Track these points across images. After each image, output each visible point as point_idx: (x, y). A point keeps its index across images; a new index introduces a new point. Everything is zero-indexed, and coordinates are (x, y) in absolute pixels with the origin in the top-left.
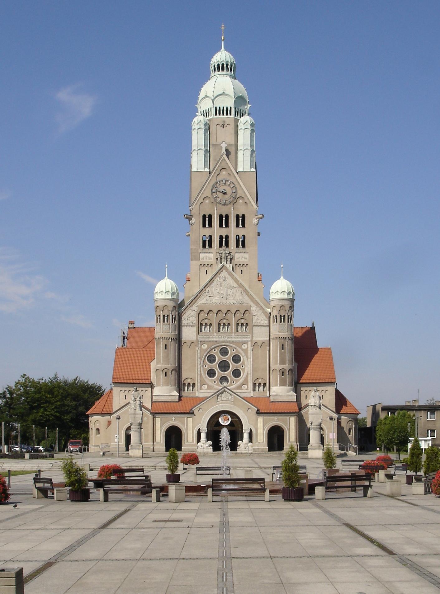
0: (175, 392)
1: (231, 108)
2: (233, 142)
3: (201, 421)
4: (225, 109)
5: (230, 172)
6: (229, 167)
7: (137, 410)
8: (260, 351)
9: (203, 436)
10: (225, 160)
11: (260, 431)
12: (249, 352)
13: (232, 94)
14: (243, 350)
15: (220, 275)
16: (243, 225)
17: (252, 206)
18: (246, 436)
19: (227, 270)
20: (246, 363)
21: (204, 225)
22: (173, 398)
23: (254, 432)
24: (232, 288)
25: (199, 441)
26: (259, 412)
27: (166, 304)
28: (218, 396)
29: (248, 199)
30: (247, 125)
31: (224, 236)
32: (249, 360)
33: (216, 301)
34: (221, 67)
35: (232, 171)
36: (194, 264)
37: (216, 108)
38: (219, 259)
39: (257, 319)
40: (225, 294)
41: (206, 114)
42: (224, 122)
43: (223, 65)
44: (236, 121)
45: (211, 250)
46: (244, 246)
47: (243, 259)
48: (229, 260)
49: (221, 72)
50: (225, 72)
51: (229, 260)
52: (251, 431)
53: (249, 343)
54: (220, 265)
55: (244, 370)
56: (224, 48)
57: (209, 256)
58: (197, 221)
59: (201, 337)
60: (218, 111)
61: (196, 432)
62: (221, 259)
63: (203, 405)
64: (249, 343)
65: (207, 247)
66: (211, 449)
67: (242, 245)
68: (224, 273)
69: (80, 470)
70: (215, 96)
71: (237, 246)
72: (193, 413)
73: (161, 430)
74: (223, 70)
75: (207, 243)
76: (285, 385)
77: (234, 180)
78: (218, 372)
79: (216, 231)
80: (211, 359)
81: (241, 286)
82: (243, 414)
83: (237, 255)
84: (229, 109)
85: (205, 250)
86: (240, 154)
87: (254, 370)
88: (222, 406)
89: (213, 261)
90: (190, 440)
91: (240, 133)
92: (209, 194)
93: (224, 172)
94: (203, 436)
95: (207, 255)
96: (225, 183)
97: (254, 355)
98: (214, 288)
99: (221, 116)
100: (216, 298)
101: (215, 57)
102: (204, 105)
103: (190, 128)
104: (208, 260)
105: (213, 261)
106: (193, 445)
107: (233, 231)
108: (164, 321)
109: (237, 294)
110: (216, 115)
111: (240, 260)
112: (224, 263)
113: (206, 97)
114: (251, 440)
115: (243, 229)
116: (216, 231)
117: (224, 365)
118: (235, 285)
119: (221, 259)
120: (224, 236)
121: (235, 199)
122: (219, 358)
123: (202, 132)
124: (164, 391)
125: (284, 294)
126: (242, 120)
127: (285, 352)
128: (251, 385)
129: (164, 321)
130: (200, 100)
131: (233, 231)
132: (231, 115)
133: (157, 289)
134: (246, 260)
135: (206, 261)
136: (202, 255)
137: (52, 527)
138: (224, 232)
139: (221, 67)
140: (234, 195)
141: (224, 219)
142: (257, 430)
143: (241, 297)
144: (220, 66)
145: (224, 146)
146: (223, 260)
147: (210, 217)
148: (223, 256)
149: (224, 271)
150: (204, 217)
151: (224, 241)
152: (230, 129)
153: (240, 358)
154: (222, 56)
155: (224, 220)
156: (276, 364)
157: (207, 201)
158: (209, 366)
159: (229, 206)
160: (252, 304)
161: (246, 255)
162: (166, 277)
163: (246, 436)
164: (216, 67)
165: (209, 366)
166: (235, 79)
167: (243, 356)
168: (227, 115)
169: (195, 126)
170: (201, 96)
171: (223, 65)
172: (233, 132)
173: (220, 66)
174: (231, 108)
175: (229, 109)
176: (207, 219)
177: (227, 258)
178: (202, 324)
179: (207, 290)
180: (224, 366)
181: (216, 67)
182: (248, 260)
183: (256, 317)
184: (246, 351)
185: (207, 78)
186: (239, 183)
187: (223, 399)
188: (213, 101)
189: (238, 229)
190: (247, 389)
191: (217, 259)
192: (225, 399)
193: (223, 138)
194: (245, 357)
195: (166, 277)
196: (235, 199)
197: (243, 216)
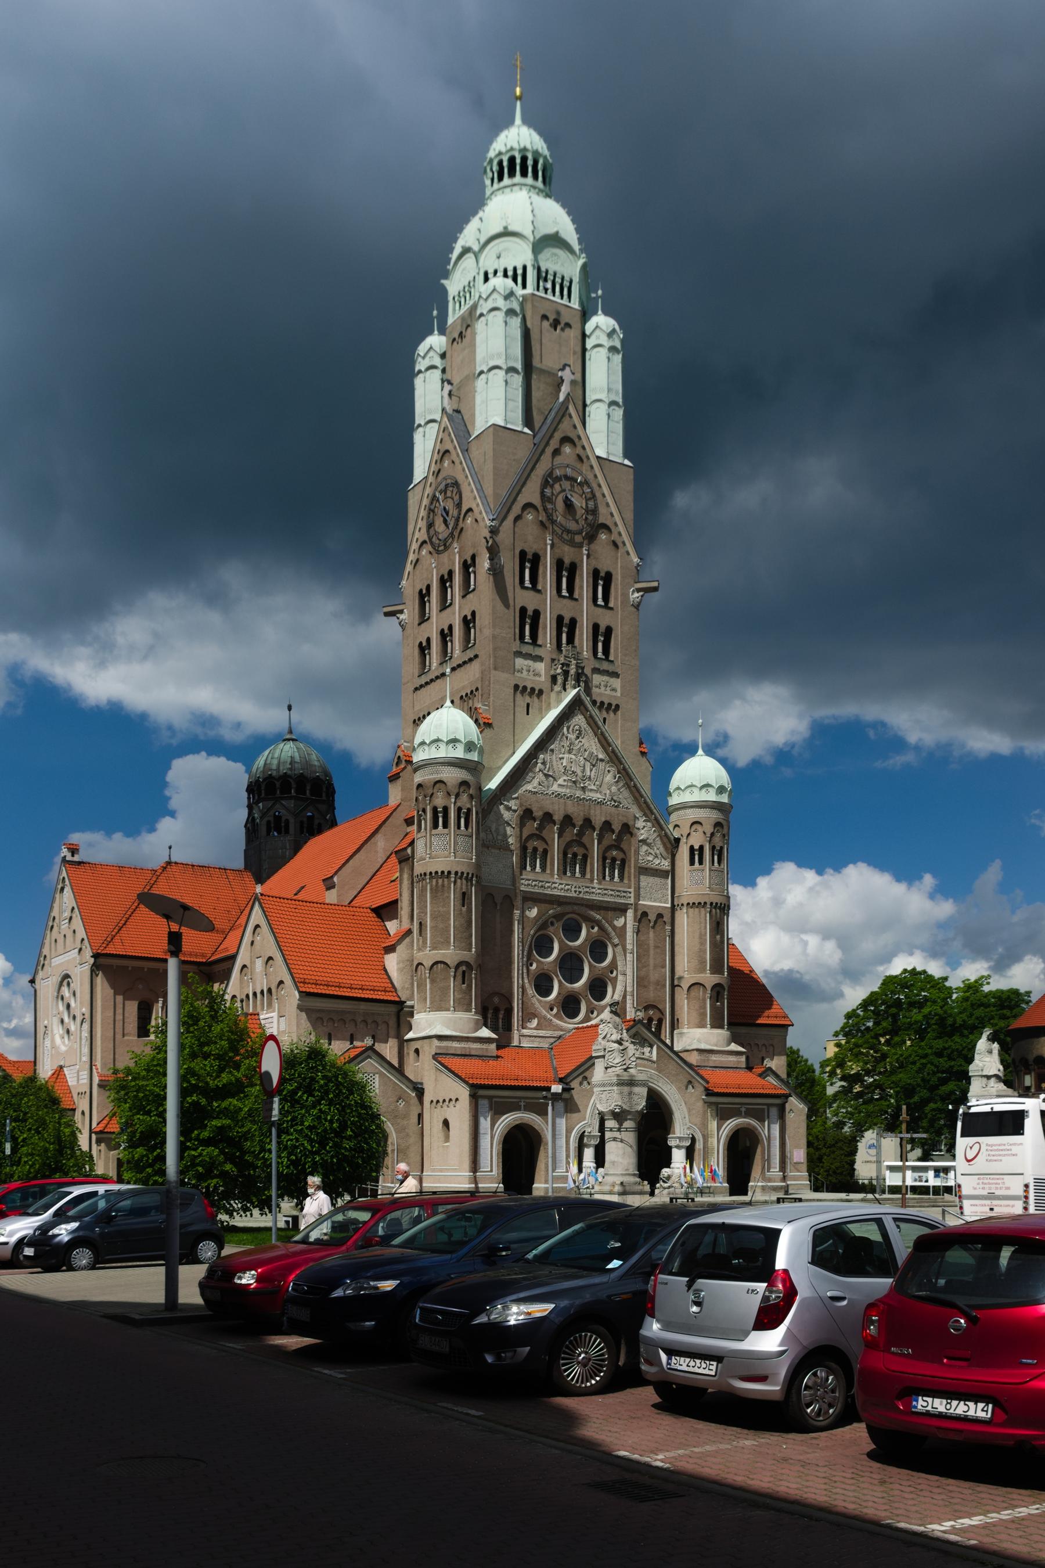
8: (651, 934)
23: (699, 1145)
24: (595, 762)
32: (629, 957)
33: (560, 790)
34: (516, 166)
38: (560, 679)
42: (558, 313)
43: (524, 159)
47: (608, 692)
50: (529, 180)
52: (693, 1140)
53: (630, 913)
55: (614, 981)
67: (604, 653)
70: (483, 240)
76: (721, 1027)
77: (590, 477)
82: (678, 1096)
87: (641, 982)
92: (536, 500)
97: (640, 944)
121: (595, 529)
125: (692, 793)
139: (516, 166)
142: (705, 1138)
150: (523, 554)
154: (519, 137)
156: (702, 970)
157: (530, 517)
164: (505, 164)
171: (512, 160)
181: (505, 164)
182: (619, 694)
184: (622, 932)
196: (595, 529)
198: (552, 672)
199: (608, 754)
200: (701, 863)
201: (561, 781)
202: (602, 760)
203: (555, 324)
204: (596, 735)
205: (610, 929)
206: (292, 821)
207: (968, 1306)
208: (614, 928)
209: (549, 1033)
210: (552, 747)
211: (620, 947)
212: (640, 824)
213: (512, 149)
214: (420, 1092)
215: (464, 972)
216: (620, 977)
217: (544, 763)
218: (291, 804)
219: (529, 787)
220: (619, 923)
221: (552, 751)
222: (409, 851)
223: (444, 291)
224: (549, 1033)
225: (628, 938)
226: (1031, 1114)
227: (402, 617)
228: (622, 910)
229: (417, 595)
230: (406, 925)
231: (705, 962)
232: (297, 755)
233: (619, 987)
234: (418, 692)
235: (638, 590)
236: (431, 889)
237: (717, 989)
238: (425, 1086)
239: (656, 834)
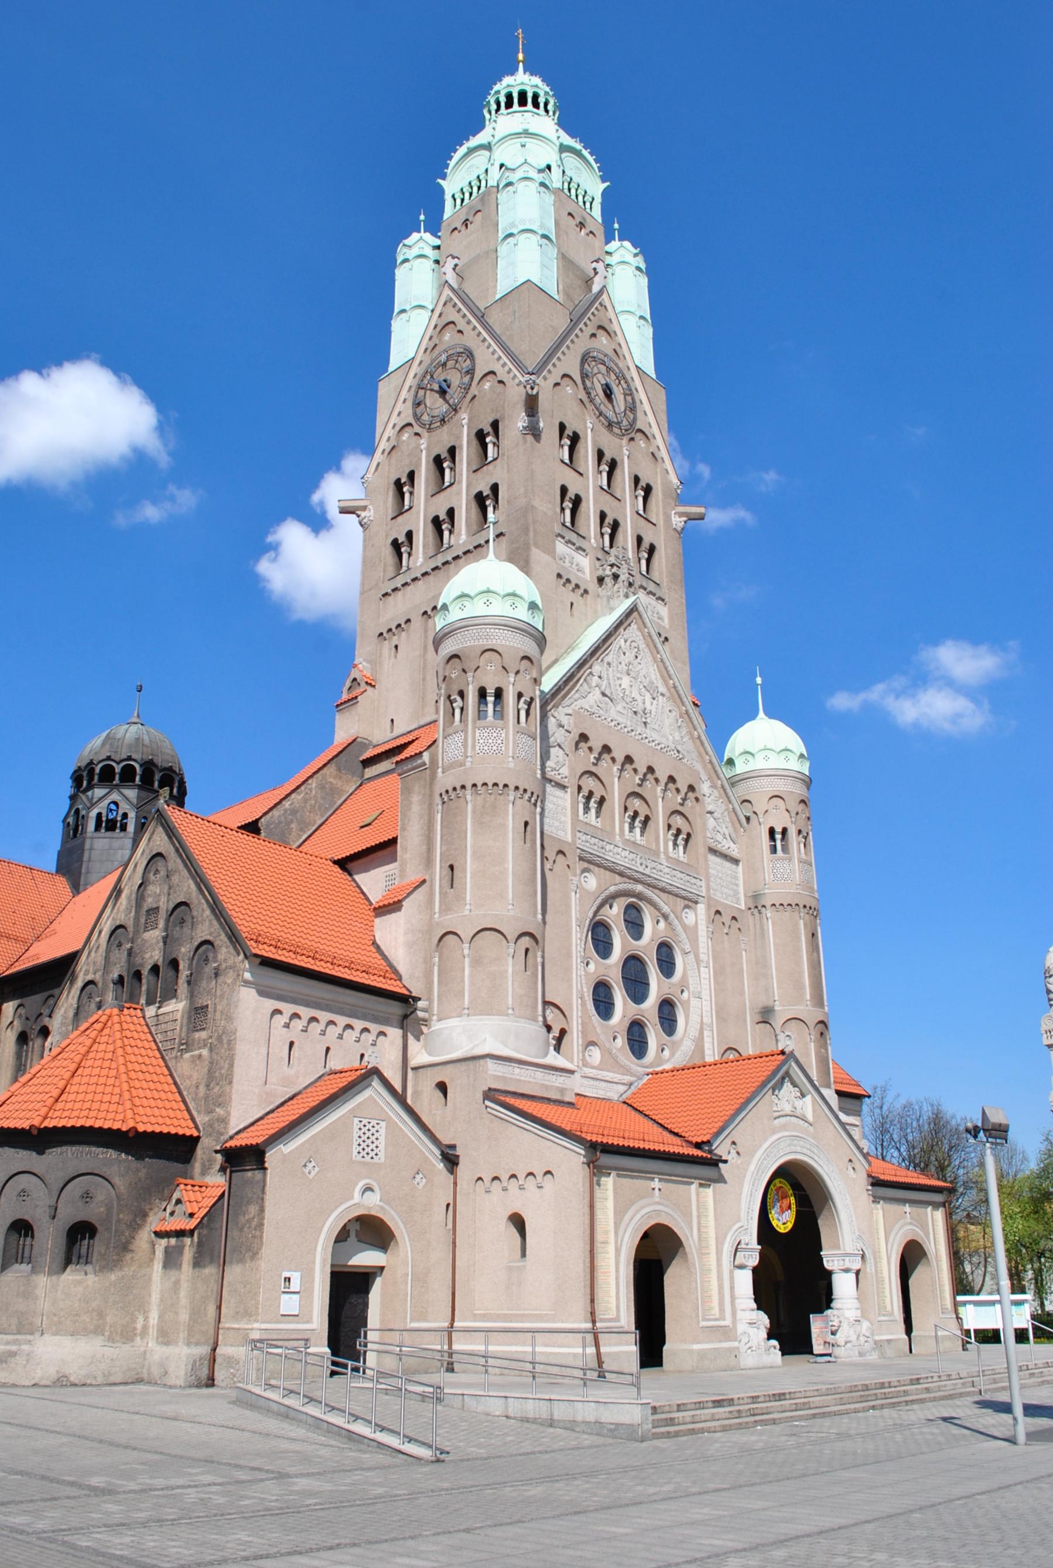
53: (701, 908)
184: (692, 932)
198: (600, 573)
199: (669, 689)
200: (785, 849)
201: (619, 708)
202: (663, 695)
204: (655, 660)
205: (679, 928)
206: (132, 815)
208: (685, 927)
209: (617, 1077)
211: (691, 956)
214: (451, 1160)
218: (132, 793)
220: (689, 917)
221: (609, 664)
222: (426, 756)
223: (441, 191)
224: (617, 1077)
225: (701, 945)
227: (363, 514)
228: (690, 902)
229: (392, 487)
230: (413, 876)
231: (803, 987)
232: (146, 737)
233: (695, 1018)
234: (389, 599)
235: (681, 515)
236: (474, 811)
238: (459, 1151)
239: (724, 807)
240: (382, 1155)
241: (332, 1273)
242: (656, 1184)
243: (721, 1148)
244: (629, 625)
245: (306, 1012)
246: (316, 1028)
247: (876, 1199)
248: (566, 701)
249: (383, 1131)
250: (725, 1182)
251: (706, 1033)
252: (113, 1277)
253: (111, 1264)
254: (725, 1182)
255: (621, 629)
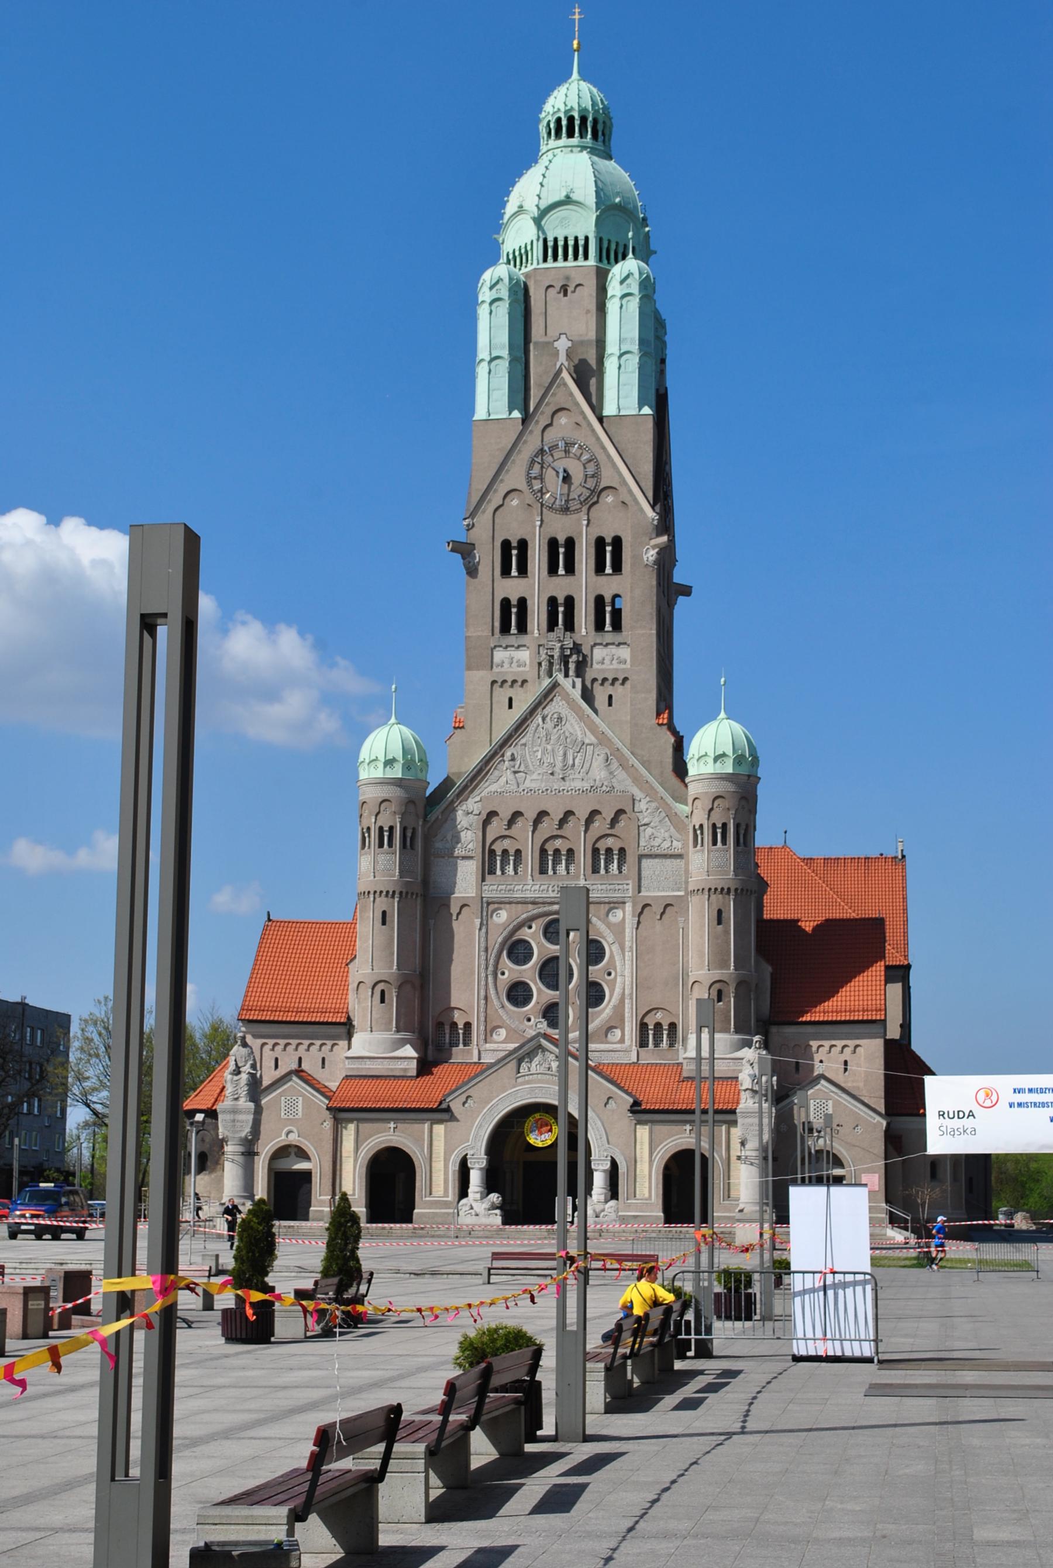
0: (408, 1047)
1: (587, 239)
2: (592, 335)
3: (471, 1136)
4: (571, 243)
5: (580, 419)
6: (577, 404)
7: (242, 1100)
9: (476, 1178)
10: (565, 384)
11: (643, 1168)
12: (627, 930)
13: (591, 200)
14: (609, 925)
15: (546, 712)
16: (617, 568)
17: (642, 510)
18: (599, 1180)
19: (567, 697)
20: (618, 964)
21: (506, 571)
22: (403, 1065)
23: (622, 1169)
25: (463, 1193)
26: (636, 1109)
27: (386, 796)
28: (520, 1061)
29: (630, 491)
30: (629, 286)
31: (561, 600)
33: (533, 785)
35: (585, 418)
36: (480, 678)
37: (545, 241)
39: (653, 837)
40: (559, 765)
41: (520, 257)
43: (571, 119)
44: (602, 276)
45: (524, 639)
46: (617, 626)
48: (572, 666)
49: (564, 140)
50: (575, 140)
51: (572, 666)
52: (614, 1164)
53: (629, 907)
54: (546, 682)
56: (579, 72)
57: (518, 658)
58: (488, 558)
59: (493, 889)
60: (552, 250)
61: (454, 1167)
62: (551, 664)
63: (477, 1091)
64: (629, 907)
65: (514, 630)
66: (496, 1218)
68: (557, 706)
69: (496, 1330)
71: (599, 626)
72: (448, 1110)
73: (356, 1160)
74: (570, 134)
75: (512, 617)
77: (591, 442)
78: (539, 990)
79: (583, 585)
80: (518, 951)
81: (603, 740)
83: (598, 653)
84: (581, 243)
85: (511, 640)
86: (611, 366)
87: (639, 984)
88: (532, 1089)
89: (528, 670)
90: (438, 1190)
91: (612, 307)
92: (522, 485)
93: (562, 420)
94: (476, 1178)
95: (612, 649)
96: (567, 452)
98: (532, 749)
99: (560, 263)
100: (535, 776)
101: (551, 100)
102: (518, 234)
103: (473, 303)
104: (515, 668)
105: (528, 670)
106: (446, 1205)
107: (536, 587)
108: (381, 845)
109: (595, 764)
110: (545, 260)
111: (607, 665)
112: (560, 677)
113: (521, 210)
114: (613, 1192)
115: (616, 578)
116: (536, 587)
117: (558, 969)
118: (590, 738)
119: (551, 664)
120: (561, 600)
122: (541, 948)
123: (503, 310)
124: (376, 1046)
126: (618, 271)
127: (728, 932)
128: (630, 1029)
129: (381, 845)
130: (506, 217)
131: (583, 585)
132: (586, 257)
133: (364, 754)
134: (622, 666)
135: (510, 671)
136: (499, 655)
137: (77, 1442)
138: (560, 587)
139: (567, 127)
140: (591, 484)
141: (562, 550)
143: (604, 774)
144: (564, 123)
145: (562, 345)
146: (556, 667)
147: (523, 545)
148: (556, 654)
149: (557, 699)
150: (506, 545)
151: (561, 613)
152: (588, 294)
153: (603, 949)
154: (571, 95)
155: (561, 555)
156: (702, 969)
158: (511, 971)
159: (574, 516)
160: (639, 794)
161: (625, 653)
162: (723, 715)
163: (599, 1180)
164: (552, 125)
165: (511, 971)
166: (610, 158)
167: (610, 945)
168: (576, 258)
169: (485, 295)
170: (510, 209)
172: (593, 307)
173: (564, 123)
174: (587, 239)
175: (581, 243)
176: (514, 552)
177: (566, 664)
178: (492, 852)
179: (508, 754)
180: (550, 972)
181: (552, 125)
182: (628, 666)
183: (649, 830)
184: (618, 930)
185: (529, 157)
186: (604, 448)
187: (533, 1071)
188: (538, 221)
189: (602, 579)
190: (622, 1041)
191: (540, 664)
192: (541, 1070)
193: (562, 327)
194: (615, 948)
195: (723, 715)
196: (595, 495)
197: (617, 542)
203: (564, 290)
207: (696, 1392)
210: (523, 741)
212: (642, 806)
213: (572, 109)
215: (383, 992)
216: (619, 979)
217: (513, 759)
219: (493, 788)
226: (316, 1179)
233: (618, 990)
237: (717, 986)
240: (300, 1114)
241: (788, 1223)
242: (392, 1125)
243: (456, 1106)
244: (552, 700)
245: (282, 1042)
246: (290, 1048)
247: (640, 1122)
248: (476, 792)
249: (300, 1102)
250: (457, 1120)
251: (627, 1001)
252: (213, 1176)
253: (213, 1171)
254: (457, 1120)
255: (540, 709)
